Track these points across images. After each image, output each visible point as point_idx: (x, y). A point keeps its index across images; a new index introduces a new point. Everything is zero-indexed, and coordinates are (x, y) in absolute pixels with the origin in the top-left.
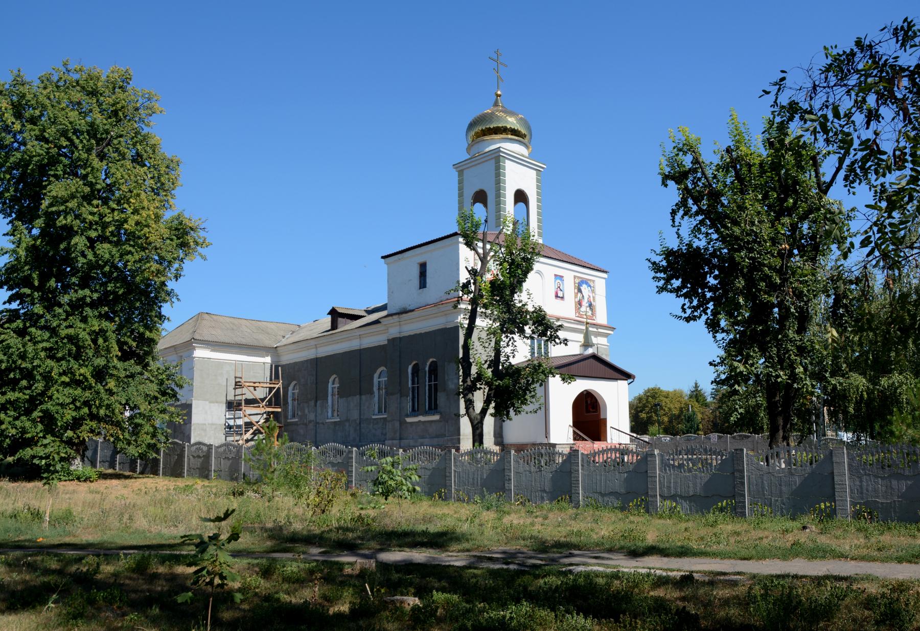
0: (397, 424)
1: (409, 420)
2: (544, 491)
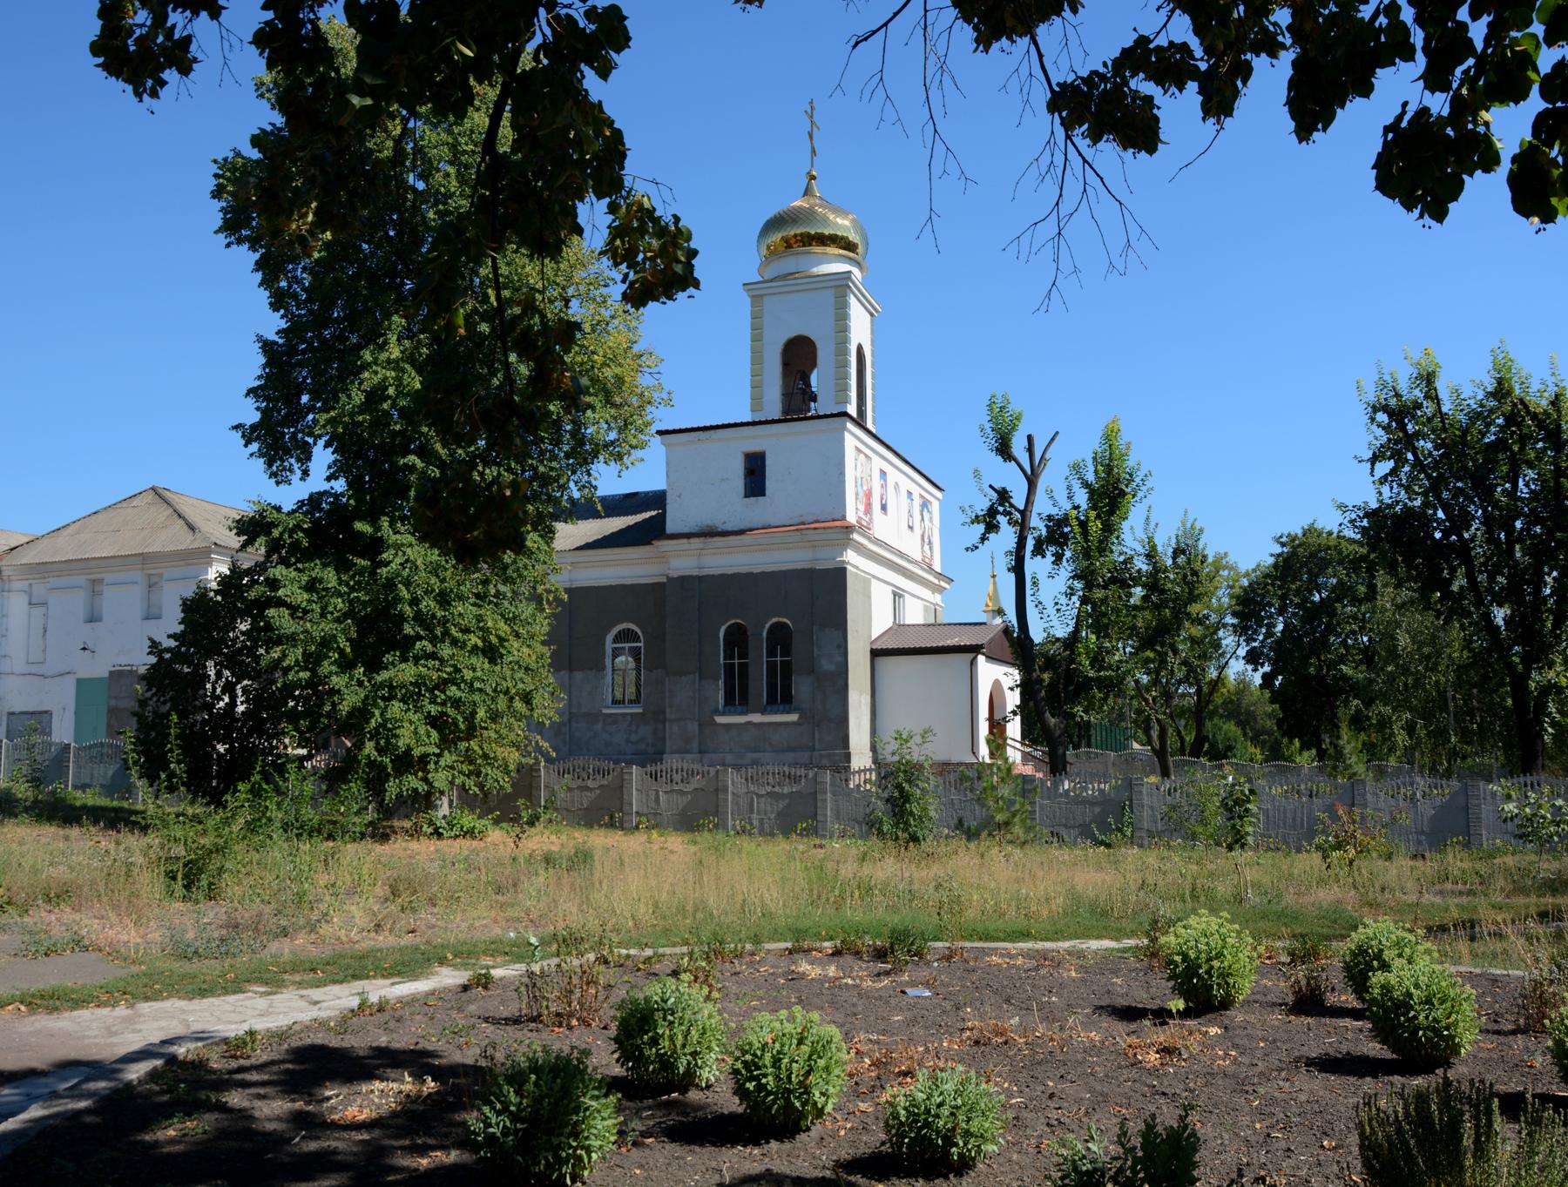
0: (693, 727)
1: (720, 720)
2: (1423, 833)
